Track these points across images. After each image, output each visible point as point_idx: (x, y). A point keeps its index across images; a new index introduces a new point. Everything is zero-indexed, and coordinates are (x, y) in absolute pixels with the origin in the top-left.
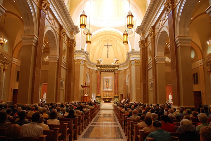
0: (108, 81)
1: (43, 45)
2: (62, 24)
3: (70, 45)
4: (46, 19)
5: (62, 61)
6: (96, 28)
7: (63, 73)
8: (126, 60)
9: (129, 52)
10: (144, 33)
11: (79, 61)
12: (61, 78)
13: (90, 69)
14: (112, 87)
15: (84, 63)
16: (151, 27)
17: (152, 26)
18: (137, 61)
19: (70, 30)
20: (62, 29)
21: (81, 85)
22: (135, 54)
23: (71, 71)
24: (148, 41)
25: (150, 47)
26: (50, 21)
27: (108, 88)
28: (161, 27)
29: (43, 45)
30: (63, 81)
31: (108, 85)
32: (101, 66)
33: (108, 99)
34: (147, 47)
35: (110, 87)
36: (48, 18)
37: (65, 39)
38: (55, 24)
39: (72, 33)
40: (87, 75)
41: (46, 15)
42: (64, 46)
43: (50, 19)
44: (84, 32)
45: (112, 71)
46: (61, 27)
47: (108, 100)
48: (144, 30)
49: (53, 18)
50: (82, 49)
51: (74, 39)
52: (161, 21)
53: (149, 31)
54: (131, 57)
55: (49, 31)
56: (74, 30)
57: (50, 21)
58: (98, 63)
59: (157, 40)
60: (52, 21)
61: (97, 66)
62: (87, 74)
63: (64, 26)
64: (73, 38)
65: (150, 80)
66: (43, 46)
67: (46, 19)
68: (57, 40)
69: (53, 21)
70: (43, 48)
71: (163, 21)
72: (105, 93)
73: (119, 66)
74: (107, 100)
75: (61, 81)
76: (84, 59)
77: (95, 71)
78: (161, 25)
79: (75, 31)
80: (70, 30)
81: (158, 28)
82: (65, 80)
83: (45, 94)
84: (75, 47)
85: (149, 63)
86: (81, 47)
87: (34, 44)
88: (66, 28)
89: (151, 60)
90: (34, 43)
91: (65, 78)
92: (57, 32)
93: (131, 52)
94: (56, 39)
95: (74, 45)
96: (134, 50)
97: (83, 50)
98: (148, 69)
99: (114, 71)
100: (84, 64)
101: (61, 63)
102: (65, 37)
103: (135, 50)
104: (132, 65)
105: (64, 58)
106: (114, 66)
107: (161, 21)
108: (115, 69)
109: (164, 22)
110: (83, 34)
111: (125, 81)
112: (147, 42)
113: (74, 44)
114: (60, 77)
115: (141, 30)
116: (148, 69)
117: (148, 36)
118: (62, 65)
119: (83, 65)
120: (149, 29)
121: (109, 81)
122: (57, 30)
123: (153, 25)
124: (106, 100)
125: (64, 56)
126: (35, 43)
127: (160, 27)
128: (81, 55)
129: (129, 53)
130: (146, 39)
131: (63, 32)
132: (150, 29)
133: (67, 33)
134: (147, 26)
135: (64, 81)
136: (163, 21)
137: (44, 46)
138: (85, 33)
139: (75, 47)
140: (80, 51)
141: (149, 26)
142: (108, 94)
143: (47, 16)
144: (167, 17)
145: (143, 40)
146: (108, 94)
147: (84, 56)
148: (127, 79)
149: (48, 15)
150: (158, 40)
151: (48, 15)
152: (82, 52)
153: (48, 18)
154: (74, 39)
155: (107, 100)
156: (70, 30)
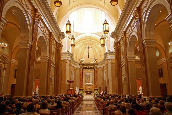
1: (36, 48)
2: (51, 31)
7: (52, 70)
10: (117, 37)
13: (74, 67)
16: (123, 33)
25: (123, 48)
26: (42, 29)
30: (52, 78)
34: (120, 49)
36: (40, 27)
37: (54, 43)
42: (53, 49)
43: (42, 27)
45: (92, 69)
50: (67, 51)
54: (108, 56)
55: (41, 37)
56: (61, 35)
57: (42, 29)
58: (81, 62)
69: (44, 29)
70: (36, 51)
75: (51, 77)
78: (131, 30)
79: (62, 37)
81: (129, 33)
82: (54, 76)
88: (55, 34)
89: (124, 59)
94: (46, 42)
97: (69, 51)
103: (110, 51)
106: (93, 65)
108: (95, 67)
112: (120, 45)
114: (50, 74)
117: (121, 40)
118: (51, 64)
122: (47, 36)
125: (53, 56)
127: (130, 32)
130: (119, 42)
131: (52, 38)
143: (39, 25)
144: (135, 24)
147: (69, 57)
149: (40, 24)
151: (40, 24)
153: (40, 27)
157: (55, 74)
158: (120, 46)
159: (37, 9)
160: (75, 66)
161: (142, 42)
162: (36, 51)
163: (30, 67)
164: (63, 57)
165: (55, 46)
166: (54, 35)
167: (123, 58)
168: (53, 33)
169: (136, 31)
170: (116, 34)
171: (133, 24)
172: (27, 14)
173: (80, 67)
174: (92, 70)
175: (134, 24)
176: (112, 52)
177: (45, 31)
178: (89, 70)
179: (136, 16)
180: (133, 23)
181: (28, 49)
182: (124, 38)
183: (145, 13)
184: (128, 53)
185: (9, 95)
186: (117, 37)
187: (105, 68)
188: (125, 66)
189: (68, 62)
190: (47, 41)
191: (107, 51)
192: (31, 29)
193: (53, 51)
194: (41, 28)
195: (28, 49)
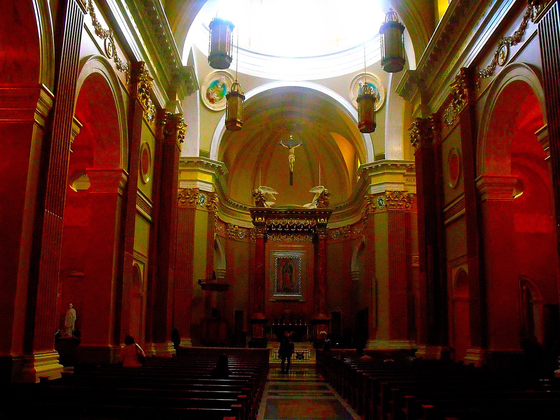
1: (74, 125)
2: (139, 57)
3: (165, 133)
4: (84, 29)
5: (138, 192)
6: (254, 81)
7: (141, 232)
8: (351, 197)
9: (367, 165)
10: (427, 98)
11: (195, 192)
12: (135, 255)
13: (226, 224)
15: (208, 202)
16: (458, 72)
17: (463, 69)
18: (395, 195)
19: (168, 82)
20: (142, 72)
21: (200, 281)
22: (386, 171)
23: (542, 86)
24: (446, 122)
25: (453, 143)
26: (100, 42)
28: (503, 68)
29: (74, 125)
30: (141, 267)
32: (270, 214)
34: (440, 146)
36: (92, 29)
37: (150, 113)
38: (115, 54)
39: (171, 94)
40: (216, 246)
41: (85, 13)
42: (147, 138)
43: (98, 32)
44: (208, 95)
45: (303, 233)
46: (135, 68)
48: (428, 86)
49: (110, 31)
50: (201, 153)
51: (180, 114)
52: (505, 49)
53: (451, 85)
54: (374, 181)
55: (95, 78)
56: (178, 79)
57: (100, 42)
58: (257, 203)
59: (484, 118)
60: (105, 40)
61: (255, 214)
62: (218, 241)
63: (145, 64)
64: (177, 112)
65: (451, 261)
66: (74, 131)
67: (84, 29)
68: (123, 113)
69: (108, 41)
70: (72, 138)
71: (512, 48)
73: (331, 212)
75: (134, 262)
76: (210, 188)
77: (244, 230)
78: (501, 61)
79: (182, 88)
80: (165, 83)
81: (491, 74)
82: (146, 261)
83: (73, 311)
84: (181, 141)
85: (446, 203)
86: (198, 147)
87: (41, 119)
88: (153, 72)
89: (461, 190)
90: (38, 113)
91: (146, 255)
92: (120, 80)
93: (373, 166)
94: (117, 105)
95: (179, 137)
96: (382, 156)
97: (207, 155)
98: (447, 222)
99: (309, 233)
100: (207, 206)
101: (136, 198)
102: (149, 104)
103: (387, 158)
104: (375, 208)
105: (144, 183)
106: (312, 214)
107: (505, 49)
108: (318, 224)
109: (514, 49)
110: (208, 101)
111: (347, 266)
112: (439, 128)
113: (181, 133)
114: (131, 250)
115: (418, 85)
116: (447, 222)
117: (445, 105)
118: (138, 207)
119: (205, 209)
120: (453, 79)
122: (121, 75)
123: (467, 63)
125: (146, 172)
126: (42, 116)
127: (499, 70)
128: (199, 174)
129: (367, 168)
130: (438, 116)
131: (143, 86)
132: (458, 77)
133: (155, 92)
134: (444, 65)
135: (141, 262)
136: (512, 48)
137: (78, 130)
138: (212, 97)
139: (181, 141)
140: (195, 161)
141: (452, 66)
143: (87, 19)
144: (532, 28)
145: (425, 119)
147: (209, 178)
148: (357, 257)
149: (93, 15)
150: (488, 118)
151: (93, 15)
152: (201, 163)
153: (92, 29)
154: (180, 114)
156: (168, 82)
157: (150, 251)
158: (439, 135)
159: (141, 63)
160: (232, 221)
161: (476, 182)
162: (72, 138)
163: (126, 253)
164: (185, 181)
165: (152, 126)
166: (151, 76)
167: (456, 187)
168: (146, 67)
169: (537, 62)
170: (422, 80)
171: (517, 29)
172: (119, 89)
173: (252, 226)
174: (303, 239)
175: (495, 63)
176: (395, 165)
177: (111, 53)
178: (289, 239)
179: (460, 93)
180: (516, 27)
181: (119, 197)
182: (463, 97)
183: (488, 92)
184: (482, 159)
185: (479, 361)
186: (427, 98)
187: (357, 230)
188: (463, 225)
189: (201, 202)
190: (120, 97)
191: (371, 159)
192: (125, 136)
193: (145, 147)
194: (95, 36)
195: (35, 127)
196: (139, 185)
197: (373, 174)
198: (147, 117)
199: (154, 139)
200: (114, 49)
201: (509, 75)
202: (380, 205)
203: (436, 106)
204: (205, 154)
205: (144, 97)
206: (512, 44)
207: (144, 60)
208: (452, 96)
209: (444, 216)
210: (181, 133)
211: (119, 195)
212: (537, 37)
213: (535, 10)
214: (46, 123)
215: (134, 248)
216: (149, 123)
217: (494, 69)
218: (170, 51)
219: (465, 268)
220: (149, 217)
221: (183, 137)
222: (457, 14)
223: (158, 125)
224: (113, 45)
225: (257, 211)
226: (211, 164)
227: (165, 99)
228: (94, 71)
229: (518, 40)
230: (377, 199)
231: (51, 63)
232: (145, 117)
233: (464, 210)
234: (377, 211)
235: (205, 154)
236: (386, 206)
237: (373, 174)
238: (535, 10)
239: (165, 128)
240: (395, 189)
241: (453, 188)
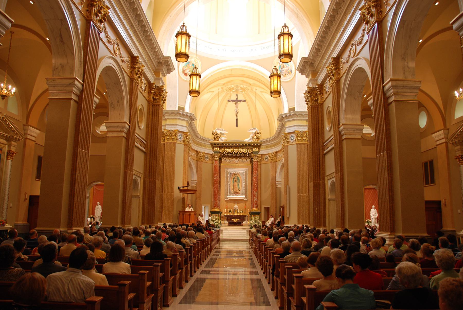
0: (236, 178)
2: (135, 54)
3: (153, 98)
4: (100, 41)
5: (136, 135)
7: (139, 160)
10: (315, 73)
11: (174, 133)
12: (134, 172)
13: (197, 151)
14: (246, 192)
15: (184, 138)
16: (330, 60)
17: (333, 58)
22: (295, 118)
25: (329, 103)
27: (236, 193)
29: (95, 99)
30: (139, 179)
31: (237, 186)
32: (222, 146)
33: (238, 218)
34: (322, 104)
35: (241, 192)
36: (105, 40)
37: (144, 85)
38: (120, 53)
39: (157, 73)
40: (190, 165)
42: (141, 102)
43: (109, 42)
44: (183, 71)
47: (237, 220)
48: (316, 67)
51: (162, 86)
52: (354, 47)
53: (327, 68)
54: (288, 125)
55: (108, 69)
58: (215, 139)
59: (344, 88)
63: (140, 57)
66: (95, 102)
67: (100, 41)
69: (116, 46)
70: (94, 106)
71: (357, 47)
72: (230, 204)
73: (261, 144)
74: (235, 221)
75: (134, 177)
77: (209, 156)
78: (352, 54)
79: (164, 68)
80: (153, 67)
81: (347, 62)
82: (142, 176)
84: (164, 102)
88: (145, 62)
89: (332, 133)
90: (74, 93)
93: (287, 115)
95: (162, 100)
98: (325, 152)
99: (249, 157)
100: (184, 141)
102: (143, 81)
103: (296, 110)
104: (288, 142)
105: (140, 129)
106: (250, 146)
107: (354, 47)
110: (183, 74)
111: (274, 178)
113: (163, 97)
114: (132, 170)
115: (310, 67)
116: (325, 152)
117: (325, 80)
118: (136, 144)
119: (182, 143)
121: (238, 179)
122: (125, 66)
123: (335, 55)
124: (233, 219)
125: (141, 122)
126: (77, 95)
127: (351, 60)
128: (178, 121)
130: (321, 86)
131: (138, 71)
132: (330, 63)
133: (147, 74)
136: (357, 47)
138: (186, 72)
140: (176, 112)
142: (236, 206)
143: (103, 35)
146: (236, 206)
147: (184, 123)
149: (106, 32)
151: (106, 32)
152: (179, 114)
153: (105, 40)
154: (162, 86)
155: (235, 221)
164: (167, 125)
165: (146, 94)
167: (330, 131)
168: (140, 59)
169: (368, 56)
170: (312, 64)
173: (212, 152)
174: (244, 160)
176: (301, 114)
177: (118, 53)
182: (333, 75)
190: (124, 78)
196: (137, 130)
197: (287, 120)
198: (142, 89)
199: (146, 102)
200: (120, 50)
201: (356, 64)
202: (292, 140)
203: (320, 79)
204: (181, 109)
205: (139, 77)
206: (357, 45)
207: (139, 55)
208: (327, 76)
209: (324, 148)
210: (163, 97)
211: (124, 137)
212: (368, 43)
213: (367, 27)
214: (79, 99)
215: (134, 168)
216: (143, 93)
217: (349, 59)
218: (155, 48)
219: (334, 179)
220: (144, 150)
221: (165, 100)
222: (328, 24)
223: (150, 92)
224: (119, 48)
225: (215, 144)
226: (186, 114)
227: (153, 77)
228: (107, 65)
229: (360, 43)
230: (290, 136)
231: (81, 64)
232: (140, 89)
233: (333, 145)
234: (290, 143)
235: (181, 109)
236: (295, 140)
237: (287, 120)
238: (367, 27)
239: (154, 95)
240: (302, 130)
241: (328, 131)
